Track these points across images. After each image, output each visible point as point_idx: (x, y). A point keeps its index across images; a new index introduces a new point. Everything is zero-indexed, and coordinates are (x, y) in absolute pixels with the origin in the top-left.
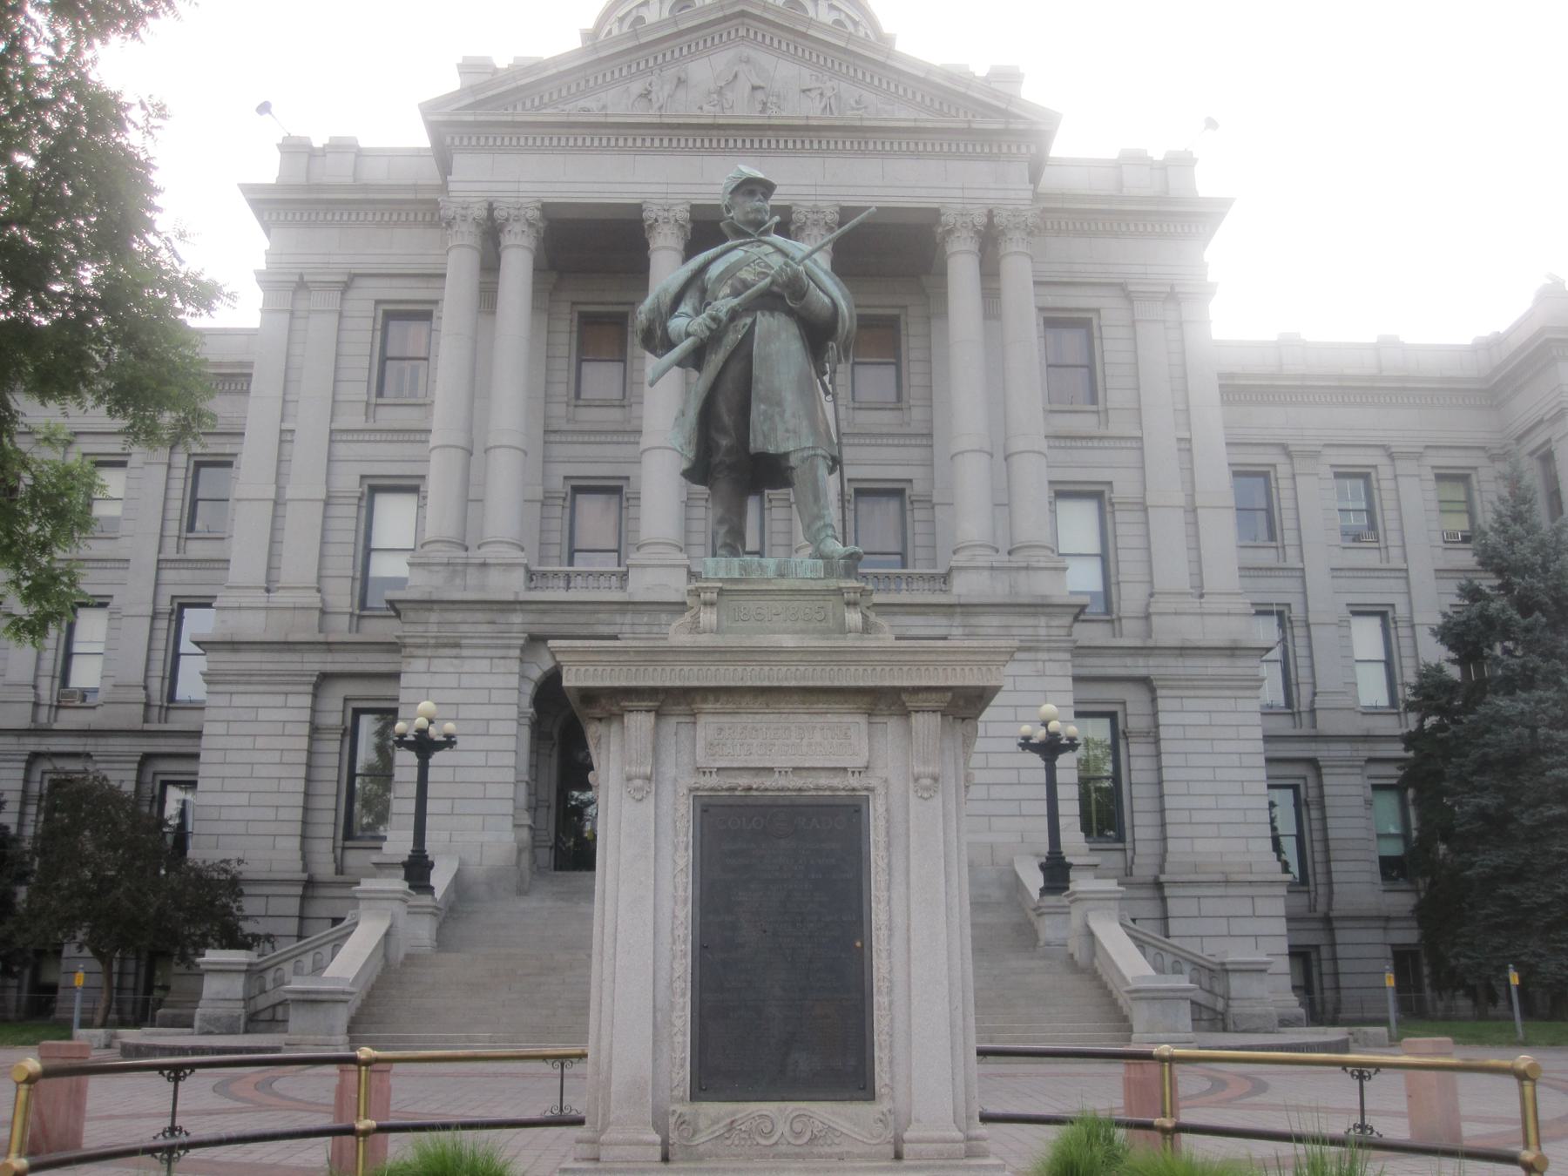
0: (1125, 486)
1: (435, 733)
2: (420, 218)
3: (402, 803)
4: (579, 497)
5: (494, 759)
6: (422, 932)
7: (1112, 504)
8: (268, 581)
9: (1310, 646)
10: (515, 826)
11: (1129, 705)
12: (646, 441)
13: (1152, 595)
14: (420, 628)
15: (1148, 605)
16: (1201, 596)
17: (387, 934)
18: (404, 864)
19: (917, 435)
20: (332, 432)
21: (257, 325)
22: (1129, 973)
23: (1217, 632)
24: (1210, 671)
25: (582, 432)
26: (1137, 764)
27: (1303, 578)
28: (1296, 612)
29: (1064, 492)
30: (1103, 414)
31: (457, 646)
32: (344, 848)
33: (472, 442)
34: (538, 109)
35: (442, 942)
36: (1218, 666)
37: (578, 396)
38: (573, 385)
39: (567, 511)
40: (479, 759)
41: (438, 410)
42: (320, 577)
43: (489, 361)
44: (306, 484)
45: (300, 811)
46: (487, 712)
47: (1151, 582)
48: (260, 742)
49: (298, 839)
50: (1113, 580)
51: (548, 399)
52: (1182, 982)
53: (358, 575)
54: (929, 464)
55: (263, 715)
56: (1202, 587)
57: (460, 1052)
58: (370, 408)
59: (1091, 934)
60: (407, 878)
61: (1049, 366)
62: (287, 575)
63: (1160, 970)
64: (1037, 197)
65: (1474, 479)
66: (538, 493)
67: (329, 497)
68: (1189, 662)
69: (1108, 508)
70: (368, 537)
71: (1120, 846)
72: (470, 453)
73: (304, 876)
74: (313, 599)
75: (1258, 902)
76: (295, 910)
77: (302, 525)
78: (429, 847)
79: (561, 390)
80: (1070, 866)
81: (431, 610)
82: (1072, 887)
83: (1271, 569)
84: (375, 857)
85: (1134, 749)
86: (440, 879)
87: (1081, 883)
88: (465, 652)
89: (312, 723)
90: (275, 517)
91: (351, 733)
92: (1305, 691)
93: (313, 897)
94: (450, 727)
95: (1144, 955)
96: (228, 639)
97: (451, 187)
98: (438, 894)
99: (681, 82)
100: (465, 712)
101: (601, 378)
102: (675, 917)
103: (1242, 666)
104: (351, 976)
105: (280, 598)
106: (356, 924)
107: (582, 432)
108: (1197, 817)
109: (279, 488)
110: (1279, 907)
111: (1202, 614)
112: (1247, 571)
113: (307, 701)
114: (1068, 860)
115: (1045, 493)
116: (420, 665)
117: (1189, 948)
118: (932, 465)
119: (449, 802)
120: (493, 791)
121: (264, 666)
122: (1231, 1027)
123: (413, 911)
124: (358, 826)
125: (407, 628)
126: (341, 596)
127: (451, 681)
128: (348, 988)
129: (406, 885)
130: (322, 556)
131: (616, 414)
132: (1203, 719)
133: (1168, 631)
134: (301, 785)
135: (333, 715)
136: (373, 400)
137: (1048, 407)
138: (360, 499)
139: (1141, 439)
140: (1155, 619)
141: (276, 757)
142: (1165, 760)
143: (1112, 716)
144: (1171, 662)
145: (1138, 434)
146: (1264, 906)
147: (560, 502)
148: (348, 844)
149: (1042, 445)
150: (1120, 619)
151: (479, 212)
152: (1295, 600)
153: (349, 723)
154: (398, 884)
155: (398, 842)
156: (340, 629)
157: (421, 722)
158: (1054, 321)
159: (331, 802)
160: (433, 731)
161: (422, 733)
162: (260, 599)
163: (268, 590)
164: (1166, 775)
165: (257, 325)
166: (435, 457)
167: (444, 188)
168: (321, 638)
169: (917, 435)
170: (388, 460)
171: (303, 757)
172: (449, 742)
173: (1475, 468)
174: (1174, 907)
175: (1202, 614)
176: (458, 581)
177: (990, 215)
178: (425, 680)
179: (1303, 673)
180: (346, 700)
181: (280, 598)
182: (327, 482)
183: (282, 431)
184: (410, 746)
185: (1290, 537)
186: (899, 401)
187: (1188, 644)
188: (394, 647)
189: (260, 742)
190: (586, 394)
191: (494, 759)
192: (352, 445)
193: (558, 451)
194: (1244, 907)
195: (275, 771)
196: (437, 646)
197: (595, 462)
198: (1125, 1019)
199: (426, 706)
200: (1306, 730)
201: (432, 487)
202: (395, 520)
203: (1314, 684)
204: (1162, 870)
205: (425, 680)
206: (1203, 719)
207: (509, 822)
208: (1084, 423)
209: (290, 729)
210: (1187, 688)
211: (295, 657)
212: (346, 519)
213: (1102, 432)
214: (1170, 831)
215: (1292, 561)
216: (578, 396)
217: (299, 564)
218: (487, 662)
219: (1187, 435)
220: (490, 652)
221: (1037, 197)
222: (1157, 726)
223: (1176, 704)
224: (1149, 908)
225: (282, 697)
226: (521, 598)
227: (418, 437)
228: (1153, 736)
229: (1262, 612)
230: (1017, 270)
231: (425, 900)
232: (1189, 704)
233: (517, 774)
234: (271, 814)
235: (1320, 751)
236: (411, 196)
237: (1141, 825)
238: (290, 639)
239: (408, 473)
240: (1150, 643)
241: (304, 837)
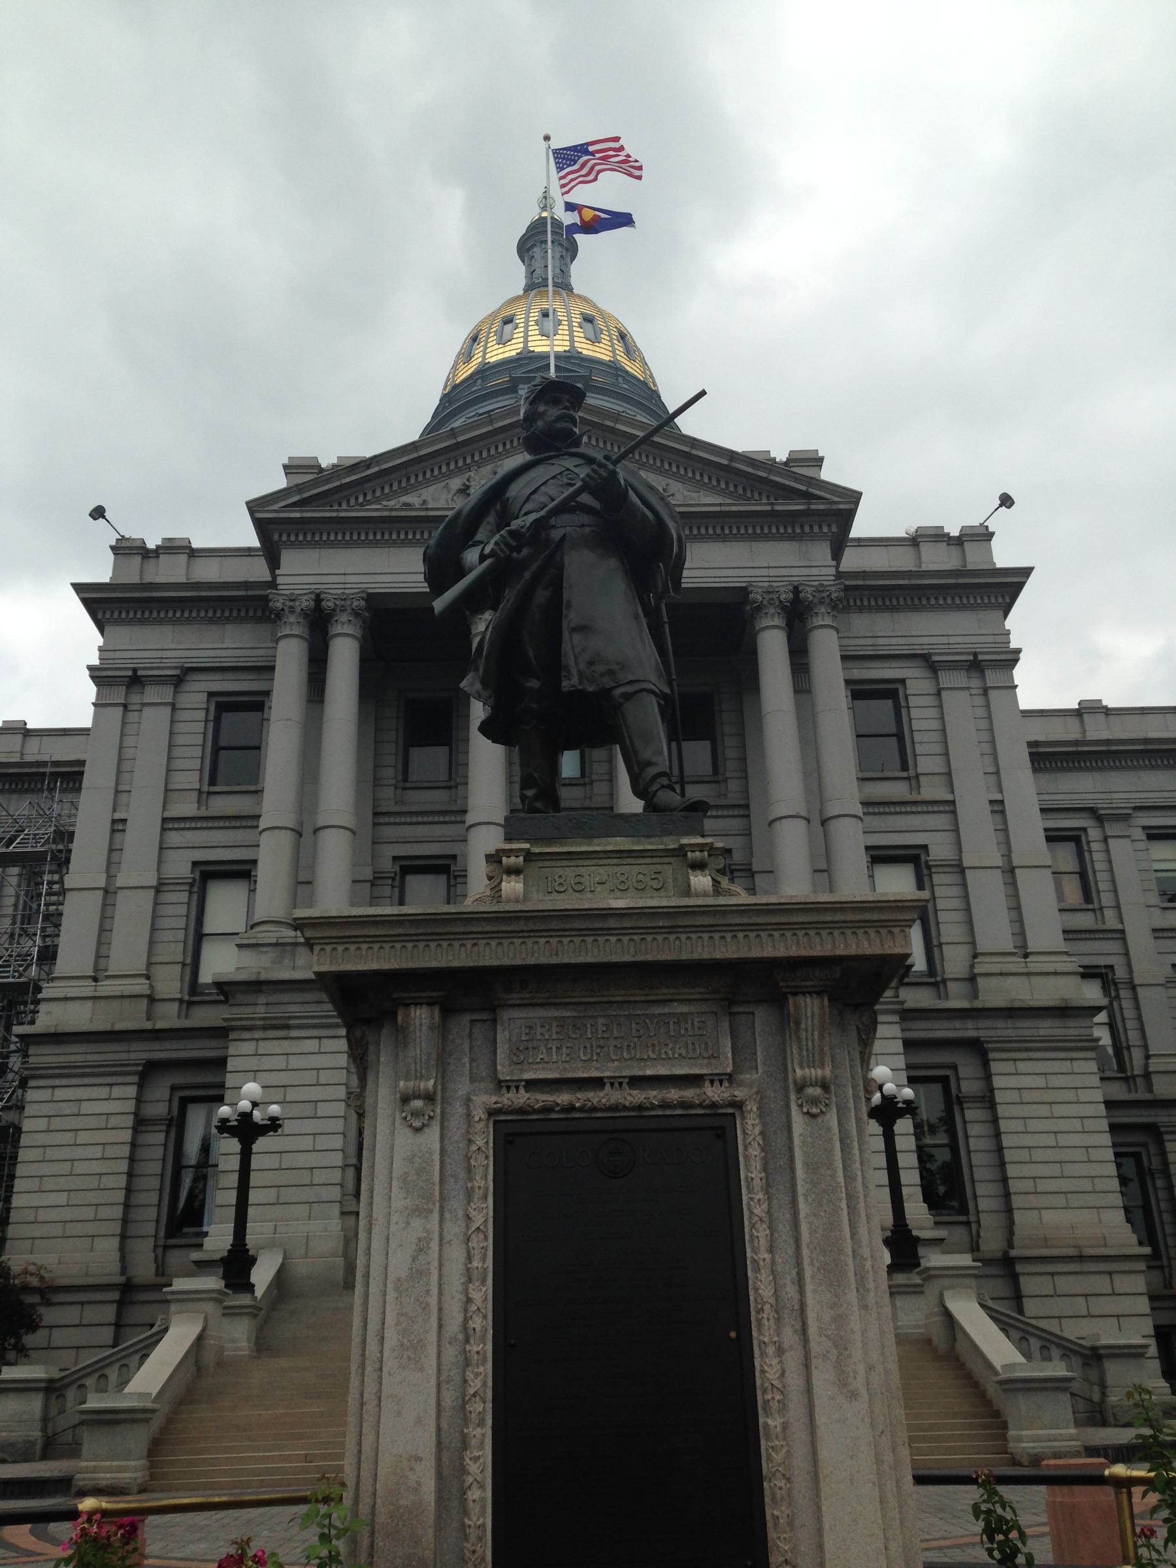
0: (940, 849)
3: (223, 1197)
4: (410, 879)
5: (323, 1143)
6: (238, 1336)
7: (929, 867)
8: (96, 970)
9: (1137, 1007)
10: (343, 1213)
11: (960, 1068)
12: (471, 818)
13: (975, 956)
14: (248, 1010)
15: (972, 966)
16: (1026, 956)
17: (200, 1338)
19: (734, 806)
20: (164, 820)
22: (997, 1362)
23: (1046, 992)
24: (1042, 1032)
25: (411, 813)
26: (974, 1130)
27: (1124, 939)
28: (1120, 973)
29: (880, 857)
30: (914, 780)
31: (287, 1027)
32: (166, 1247)
33: (302, 824)
34: (362, 505)
35: (262, 1346)
36: (1048, 1028)
37: (405, 780)
38: (400, 766)
39: (396, 890)
40: (306, 1143)
41: (268, 797)
42: (149, 964)
43: (319, 749)
44: (139, 867)
45: (120, 1208)
47: (973, 943)
48: (83, 1137)
49: (117, 1239)
50: (935, 942)
51: (377, 782)
52: (1058, 1369)
53: (189, 961)
54: (747, 833)
55: (86, 1108)
56: (1025, 946)
58: (203, 796)
59: (948, 1315)
60: (225, 1277)
61: (858, 736)
62: (116, 964)
63: (1028, 1355)
64: (839, 575)
66: (368, 874)
67: (161, 884)
68: (1020, 1023)
69: (925, 872)
70: (200, 921)
71: (963, 1218)
72: (300, 835)
73: (121, 1280)
74: (140, 986)
75: (1117, 1279)
76: (112, 1318)
77: (133, 911)
78: (251, 1239)
79: (389, 774)
80: (918, 1239)
81: (260, 991)
82: (924, 1263)
83: (1090, 931)
84: (195, 1255)
85: (970, 1114)
86: (262, 1276)
87: (933, 1259)
88: (294, 1033)
89: (136, 1114)
90: (105, 905)
92: (1137, 1055)
93: (133, 1303)
94: (274, 1109)
95: (1008, 1337)
96: (52, 1030)
97: (279, 580)
98: (259, 1292)
100: (292, 1095)
101: (429, 760)
102: (469, 1300)
103: (1072, 1029)
104: (154, 1391)
105: (108, 987)
106: (166, 1330)
107: (411, 813)
108: (1042, 1186)
109: (110, 877)
110: (1139, 1283)
111: (1028, 974)
112: (1070, 934)
113: (132, 1091)
114: (915, 1233)
115: (863, 859)
116: (248, 1048)
117: (1046, 1327)
118: (750, 835)
119: (274, 1191)
120: (320, 1177)
121: (90, 1057)
122: (1112, 1420)
123: (230, 1313)
124: (185, 1219)
125: (235, 1010)
126: (170, 983)
127: (279, 1062)
128: (149, 1405)
129: (222, 1283)
130: (152, 942)
131: (442, 795)
132: (1040, 1082)
133: (994, 994)
134: (122, 1181)
136: (206, 788)
137: (861, 776)
138: (192, 885)
139: (953, 802)
140: (981, 981)
141: (97, 1152)
142: (1004, 1125)
143: (944, 1081)
144: (1000, 1024)
145: (950, 797)
146: (1125, 1283)
147: (390, 882)
148: (172, 1242)
149: (859, 810)
150: (944, 981)
151: (306, 603)
152: (1117, 962)
153: (175, 1113)
154: (212, 1282)
155: (218, 1237)
156: (169, 1017)
157: (245, 1105)
158: (860, 692)
159: (153, 1198)
160: (257, 1114)
161: (246, 1117)
162: (86, 989)
163: (95, 979)
164: (1006, 1141)
166: (266, 840)
167: (273, 584)
168: (148, 1025)
169: (734, 806)
170: (220, 846)
171: (126, 1151)
174: (1028, 1285)
175: (1028, 974)
176: (286, 962)
177: (796, 590)
178: (252, 1064)
179: (1133, 1037)
180: (173, 1088)
181: (108, 987)
182: (158, 870)
183: (114, 821)
185: (1107, 899)
186: (717, 775)
187: (1017, 1005)
188: (221, 1033)
189: (83, 1137)
190: (414, 776)
191: (323, 1143)
192: (185, 833)
193: (389, 832)
194: (1100, 1284)
195: (96, 1167)
196: (265, 1028)
197: (424, 841)
198: (997, 1414)
199: (252, 1088)
200: (1142, 1095)
201: (262, 872)
202: (226, 907)
203: (1146, 1047)
204: (1011, 1245)
205: (252, 1064)
206: (1040, 1082)
207: (336, 1209)
208: (896, 790)
209: (113, 1121)
210: (1019, 1050)
211: (123, 1047)
212: (178, 902)
213: (915, 797)
214: (1016, 1201)
215: (1111, 921)
216: (405, 780)
217: (128, 953)
218: (316, 1041)
219: (998, 797)
220: (316, 1033)
221: (839, 575)
222: (992, 1090)
223: (1007, 1067)
224: (1000, 1287)
225: (107, 1089)
228: (988, 1100)
229: (1088, 973)
230: (826, 646)
231: (244, 1300)
232: (1022, 1066)
233: (345, 1158)
234: (89, 1213)
235: (1161, 1117)
237: (986, 1198)
238: (118, 1027)
240: (978, 1004)
241: (124, 1237)
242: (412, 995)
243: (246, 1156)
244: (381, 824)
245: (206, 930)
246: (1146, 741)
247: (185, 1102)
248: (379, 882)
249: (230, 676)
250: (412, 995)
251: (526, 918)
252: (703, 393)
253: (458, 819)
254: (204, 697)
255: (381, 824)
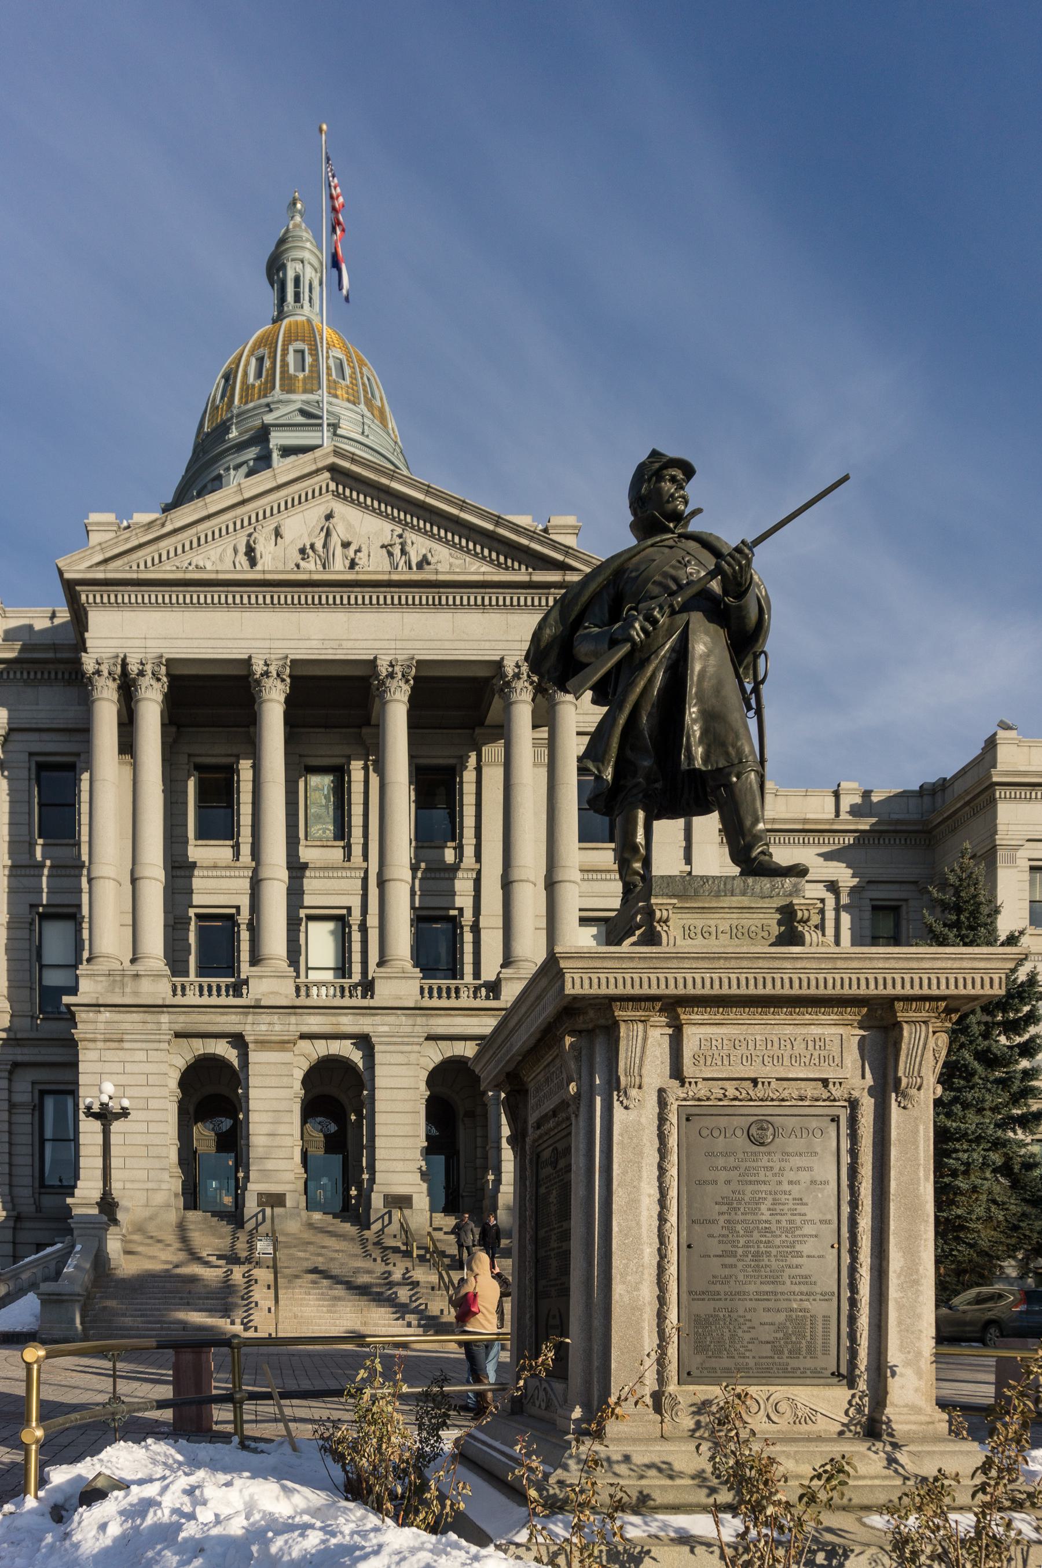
1: (114, 1106)
2: (60, 676)
18: (97, 1203)
21: (443, 1157)
32: (40, 1194)
46: (146, 1092)
57: (715, 1076)
65: (904, 909)
88: (126, 1045)
91: (39, 1109)
94: (126, 1103)
99: (278, 534)
135: (23, 1091)
153: (37, 1101)
165: (443, 1157)
172: (124, 1113)
173: (906, 900)
184: (97, 1116)
199: (109, 1088)
220: (144, 1045)
226: (167, 1003)
227: (68, 872)
236: (50, 655)
239: (66, 902)
242: (629, 1014)
243: (106, 1134)
244: (177, 877)
245: (45, 961)
246: (805, 821)
247: (43, 1093)
248: (179, 926)
249: (45, 736)
250: (629, 1014)
251: (726, 958)
252: (846, 478)
253: (36, 873)
254: (26, 757)
255: (177, 877)
